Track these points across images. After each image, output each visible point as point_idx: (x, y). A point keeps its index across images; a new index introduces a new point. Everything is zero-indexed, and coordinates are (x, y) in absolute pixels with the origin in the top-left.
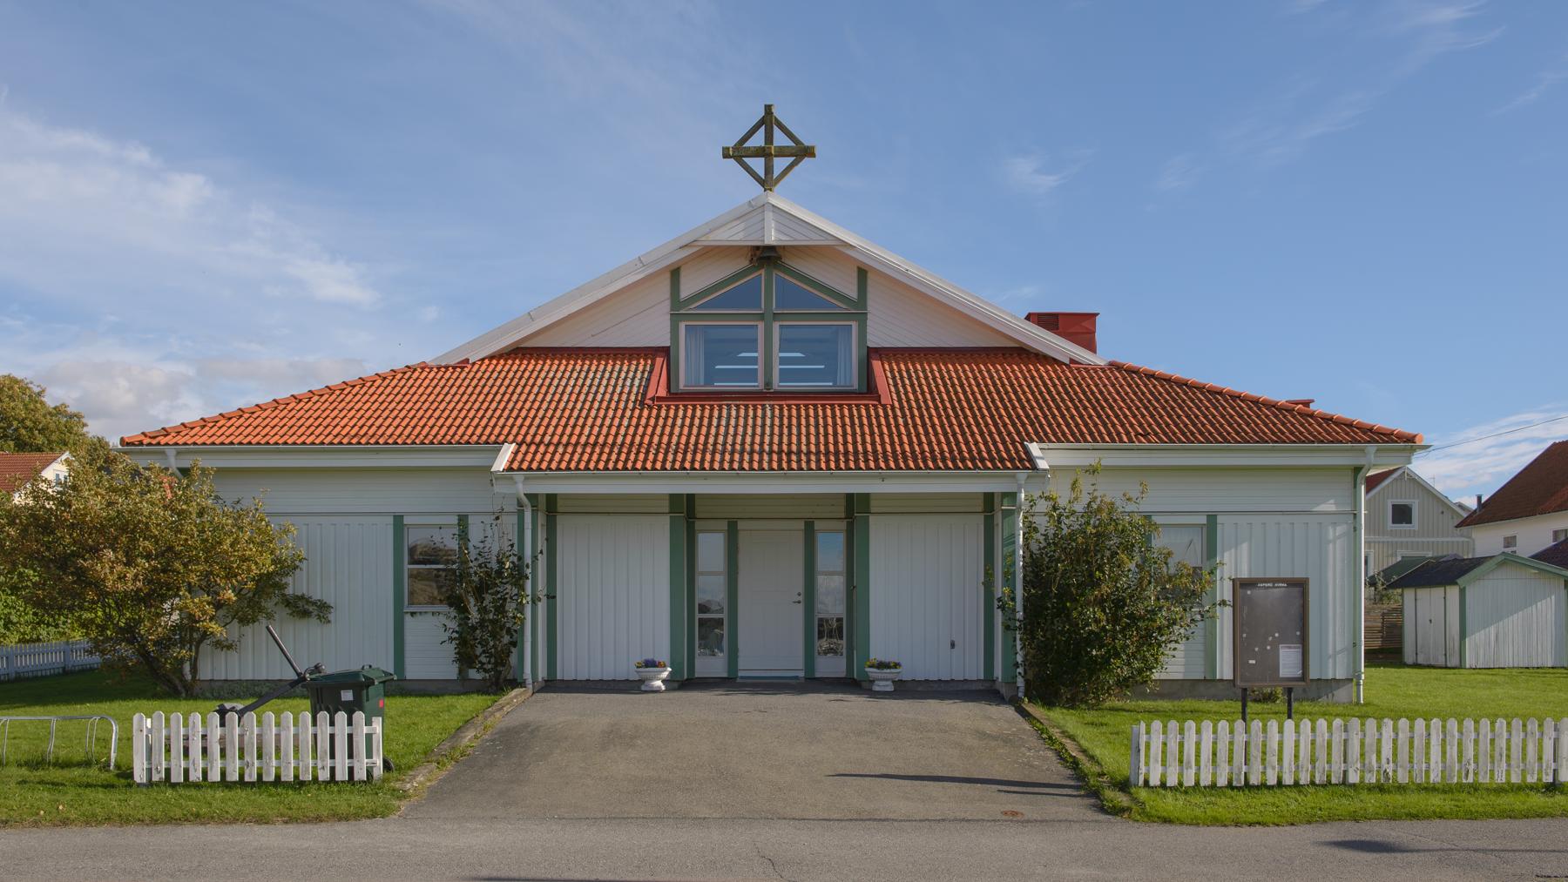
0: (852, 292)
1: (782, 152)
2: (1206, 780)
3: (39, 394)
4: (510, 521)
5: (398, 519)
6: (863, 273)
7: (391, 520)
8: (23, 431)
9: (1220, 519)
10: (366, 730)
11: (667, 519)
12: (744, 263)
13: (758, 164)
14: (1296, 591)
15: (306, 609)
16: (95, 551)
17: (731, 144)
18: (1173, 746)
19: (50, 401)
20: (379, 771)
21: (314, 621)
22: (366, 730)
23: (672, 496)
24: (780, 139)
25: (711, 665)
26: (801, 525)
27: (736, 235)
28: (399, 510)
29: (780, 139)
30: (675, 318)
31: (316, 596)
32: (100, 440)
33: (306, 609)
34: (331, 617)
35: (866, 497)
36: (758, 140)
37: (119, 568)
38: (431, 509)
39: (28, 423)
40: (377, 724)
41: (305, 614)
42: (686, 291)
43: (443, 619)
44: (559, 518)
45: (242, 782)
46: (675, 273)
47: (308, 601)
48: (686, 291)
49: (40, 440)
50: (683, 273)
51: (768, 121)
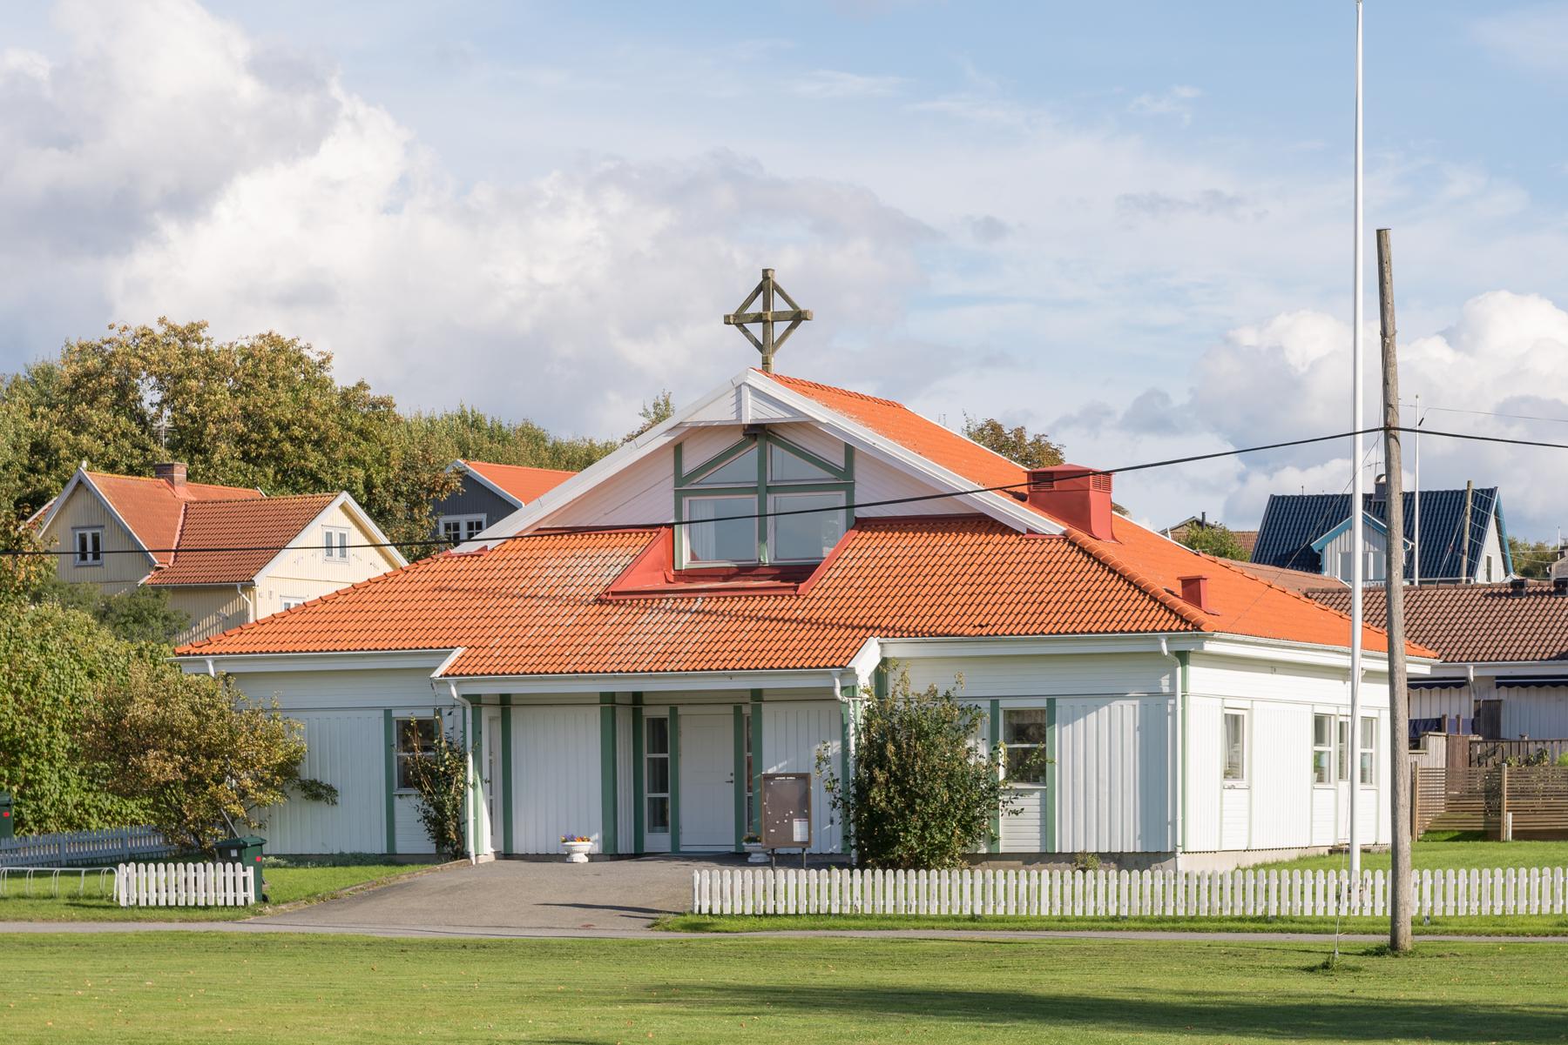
0: (840, 461)
1: (779, 317)
2: (738, 911)
3: (321, 365)
4: (458, 712)
5: (388, 712)
6: (849, 451)
7: (382, 713)
8: (287, 446)
9: (1058, 702)
10: (243, 874)
11: (598, 709)
12: (740, 437)
13: (756, 329)
14: (801, 783)
15: (318, 792)
16: (143, 750)
17: (732, 312)
18: (716, 888)
19: (341, 377)
20: (252, 900)
21: (323, 803)
22: (243, 874)
23: (602, 694)
24: (779, 305)
25: (657, 840)
26: (730, 709)
27: (722, 413)
28: (388, 704)
29: (779, 305)
30: (679, 495)
31: (327, 781)
32: (463, 418)
33: (318, 792)
34: (338, 800)
35: (760, 691)
36: (757, 307)
37: (160, 763)
38: (412, 703)
39: (297, 431)
40: (250, 871)
41: (317, 797)
42: (689, 466)
43: (419, 802)
44: (513, 710)
45: (196, 906)
46: (678, 448)
47: (320, 785)
48: (689, 466)
49: (314, 460)
50: (685, 449)
51: (766, 287)
